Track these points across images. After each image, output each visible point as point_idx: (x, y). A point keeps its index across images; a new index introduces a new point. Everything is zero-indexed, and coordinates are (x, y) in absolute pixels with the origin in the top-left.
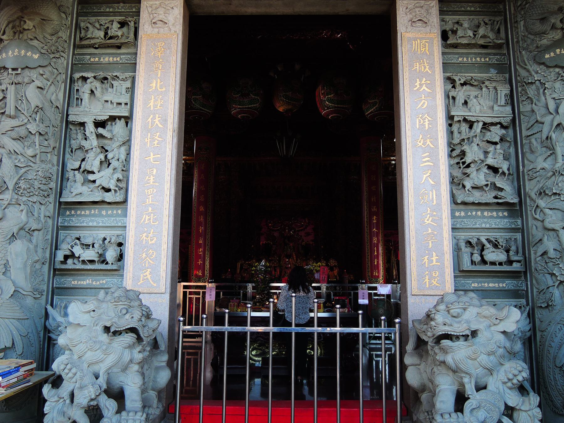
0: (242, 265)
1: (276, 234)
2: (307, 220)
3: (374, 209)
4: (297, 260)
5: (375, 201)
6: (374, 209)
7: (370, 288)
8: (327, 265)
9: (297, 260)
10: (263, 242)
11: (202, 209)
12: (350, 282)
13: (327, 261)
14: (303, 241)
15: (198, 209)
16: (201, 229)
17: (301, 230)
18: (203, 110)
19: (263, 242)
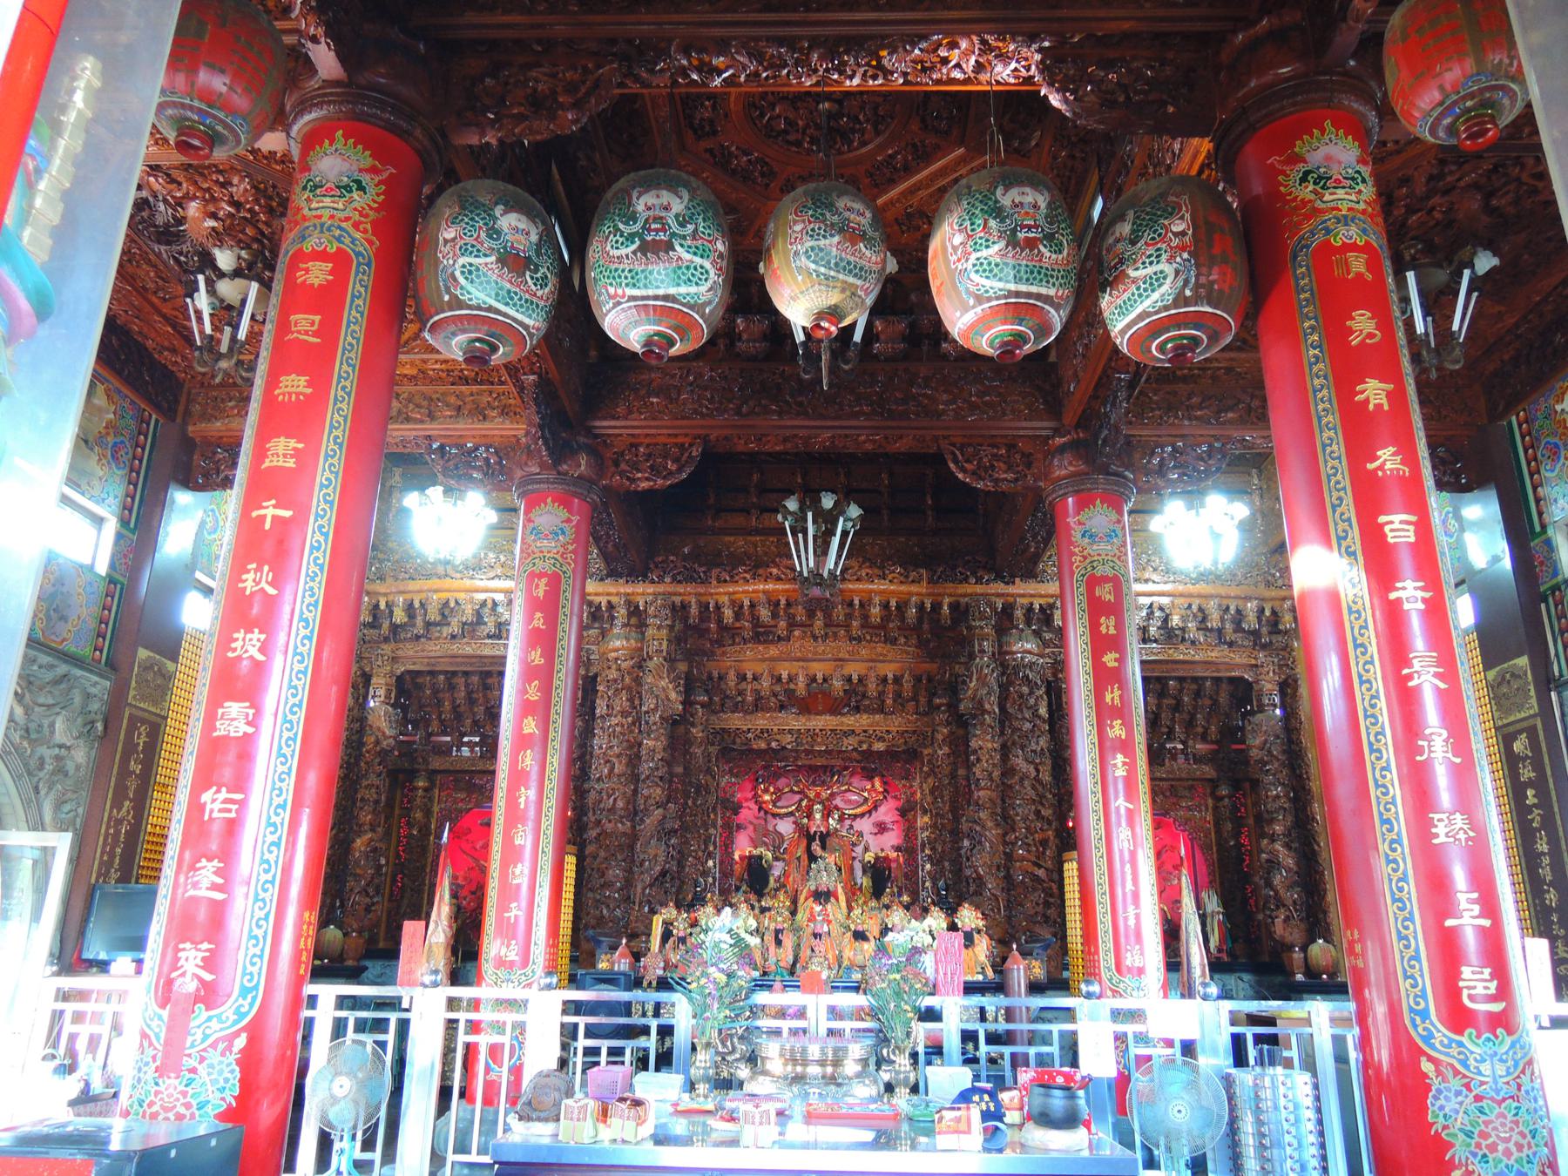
0: (668, 924)
1: (785, 827)
2: (877, 784)
3: (1387, 459)
4: (850, 909)
5: (1117, 701)
6: (1387, 459)
7: (1116, 1015)
8: (953, 927)
9: (850, 909)
10: (743, 847)
11: (530, 726)
12: (1035, 988)
13: (951, 911)
14: (866, 849)
15: (519, 727)
16: (527, 795)
17: (862, 815)
18: (505, 315)
19: (743, 847)
